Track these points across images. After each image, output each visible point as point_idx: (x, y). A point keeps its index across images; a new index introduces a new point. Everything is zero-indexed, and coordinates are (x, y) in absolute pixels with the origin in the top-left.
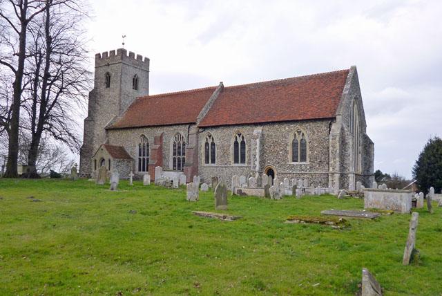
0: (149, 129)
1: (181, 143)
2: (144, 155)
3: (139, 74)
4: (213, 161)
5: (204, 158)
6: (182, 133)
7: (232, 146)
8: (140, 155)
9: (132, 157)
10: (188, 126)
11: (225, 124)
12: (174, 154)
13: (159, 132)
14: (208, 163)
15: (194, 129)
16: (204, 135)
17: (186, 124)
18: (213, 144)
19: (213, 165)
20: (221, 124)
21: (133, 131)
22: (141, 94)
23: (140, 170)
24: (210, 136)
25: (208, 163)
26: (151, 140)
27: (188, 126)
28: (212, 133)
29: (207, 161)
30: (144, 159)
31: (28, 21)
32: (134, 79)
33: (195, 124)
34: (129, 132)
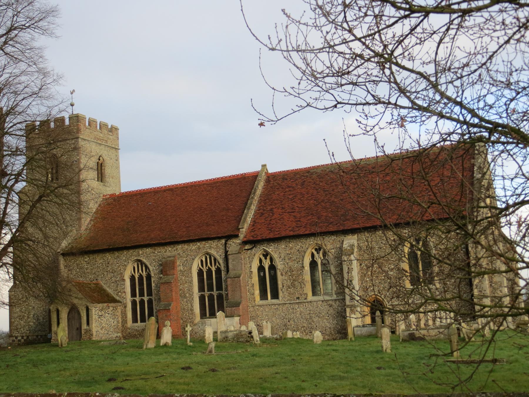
0: (148, 250)
1: (213, 269)
2: (142, 294)
3: (106, 154)
4: (275, 295)
5: (257, 292)
6: (213, 252)
7: (307, 268)
8: (133, 294)
9: (118, 298)
10: (223, 241)
11: (292, 233)
12: (201, 288)
13: (168, 252)
14: (137, 322)
15: (234, 245)
16: (258, 252)
17: (219, 238)
18: (272, 267)
19: (275, 301)
20: (283, 234)
21: (117, 254)
22: (109, 190)
23: (135, 320)
24: (265, 256)
25: (137, 322)
26: (153, 270)
27: (223, 241)
28: (269, 250)
29: (263, 296)
30: (142, 302)
31: (465, 120)
32: (98, 163)
33: (237, 236)
34: (108, 256)
